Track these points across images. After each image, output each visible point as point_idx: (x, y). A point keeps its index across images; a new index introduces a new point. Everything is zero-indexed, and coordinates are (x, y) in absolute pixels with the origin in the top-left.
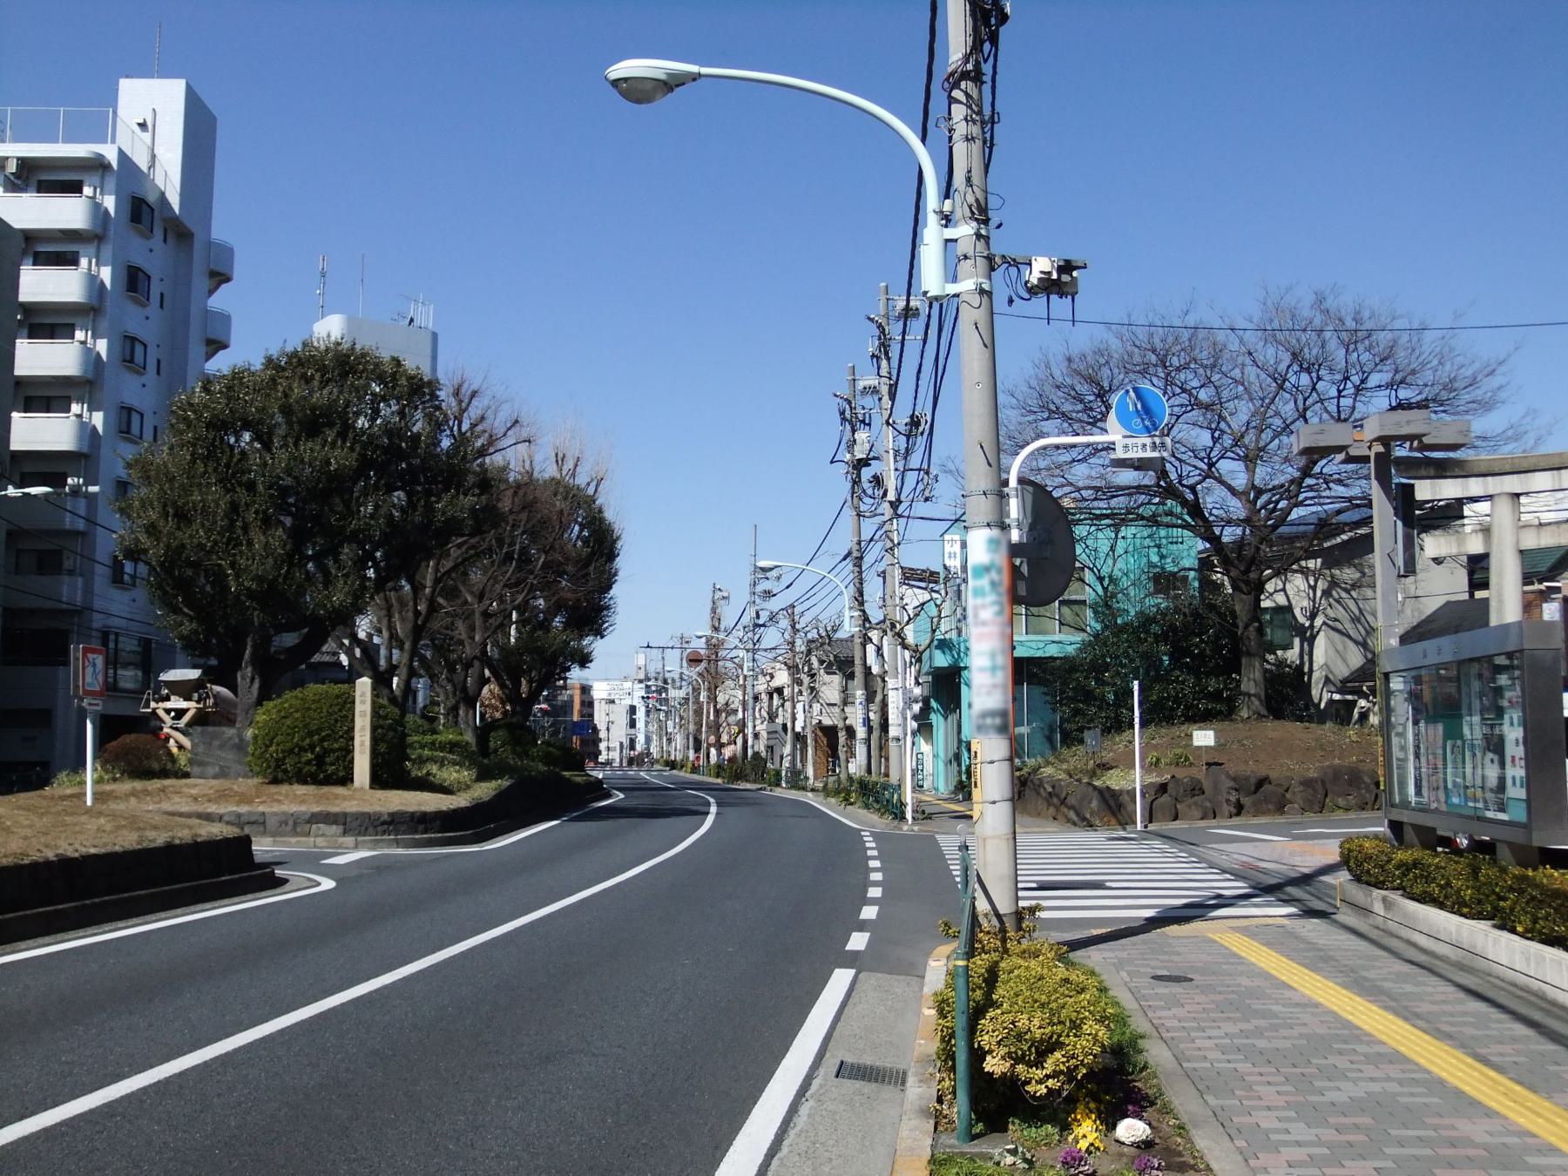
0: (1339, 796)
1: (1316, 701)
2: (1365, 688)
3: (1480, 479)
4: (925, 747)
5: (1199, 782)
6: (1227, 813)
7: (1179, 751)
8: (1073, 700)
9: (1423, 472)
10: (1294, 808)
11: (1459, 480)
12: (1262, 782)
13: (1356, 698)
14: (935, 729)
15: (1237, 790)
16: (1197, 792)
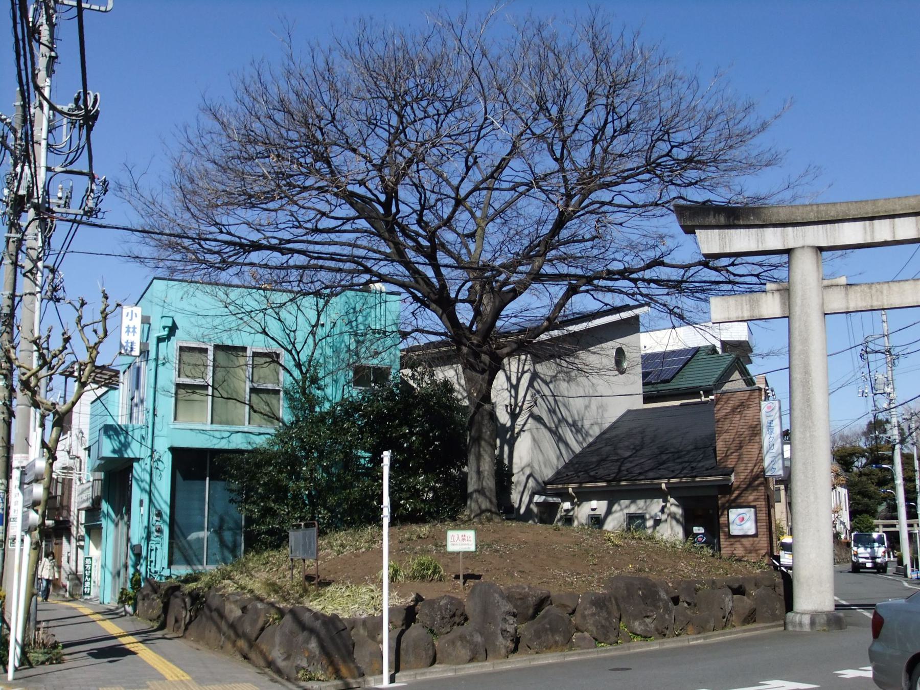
0: (635, 619)
1: (516, 505)
2: (570, 490)
3: (779, 230)
4: (94, 552)
5: (460, 603)
6: (503, 651)
7: (425, 559)
8: (263, 498)
9: (712, 220)
10: (584, 638)
11: (754, 231)
12: (543, 602)
13: (559, 500)
14: (104, 531)
15: (515, 615)
16: (457, 619)
